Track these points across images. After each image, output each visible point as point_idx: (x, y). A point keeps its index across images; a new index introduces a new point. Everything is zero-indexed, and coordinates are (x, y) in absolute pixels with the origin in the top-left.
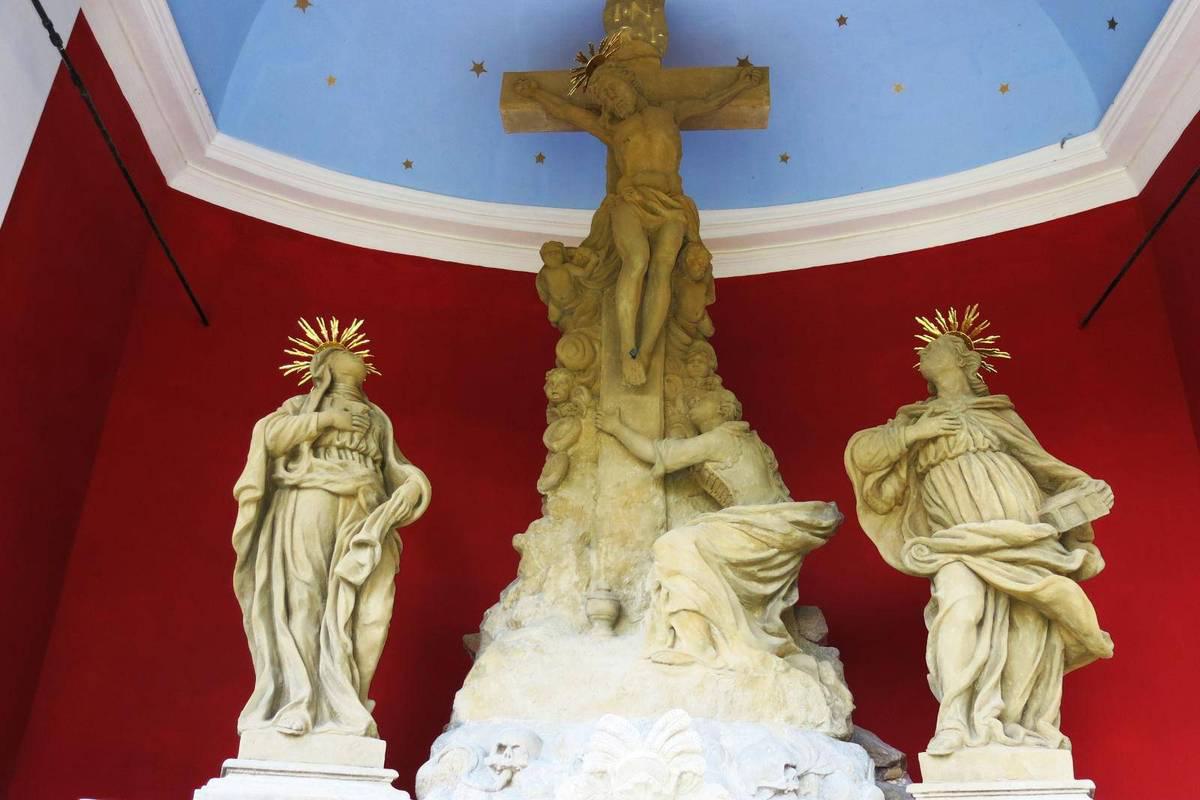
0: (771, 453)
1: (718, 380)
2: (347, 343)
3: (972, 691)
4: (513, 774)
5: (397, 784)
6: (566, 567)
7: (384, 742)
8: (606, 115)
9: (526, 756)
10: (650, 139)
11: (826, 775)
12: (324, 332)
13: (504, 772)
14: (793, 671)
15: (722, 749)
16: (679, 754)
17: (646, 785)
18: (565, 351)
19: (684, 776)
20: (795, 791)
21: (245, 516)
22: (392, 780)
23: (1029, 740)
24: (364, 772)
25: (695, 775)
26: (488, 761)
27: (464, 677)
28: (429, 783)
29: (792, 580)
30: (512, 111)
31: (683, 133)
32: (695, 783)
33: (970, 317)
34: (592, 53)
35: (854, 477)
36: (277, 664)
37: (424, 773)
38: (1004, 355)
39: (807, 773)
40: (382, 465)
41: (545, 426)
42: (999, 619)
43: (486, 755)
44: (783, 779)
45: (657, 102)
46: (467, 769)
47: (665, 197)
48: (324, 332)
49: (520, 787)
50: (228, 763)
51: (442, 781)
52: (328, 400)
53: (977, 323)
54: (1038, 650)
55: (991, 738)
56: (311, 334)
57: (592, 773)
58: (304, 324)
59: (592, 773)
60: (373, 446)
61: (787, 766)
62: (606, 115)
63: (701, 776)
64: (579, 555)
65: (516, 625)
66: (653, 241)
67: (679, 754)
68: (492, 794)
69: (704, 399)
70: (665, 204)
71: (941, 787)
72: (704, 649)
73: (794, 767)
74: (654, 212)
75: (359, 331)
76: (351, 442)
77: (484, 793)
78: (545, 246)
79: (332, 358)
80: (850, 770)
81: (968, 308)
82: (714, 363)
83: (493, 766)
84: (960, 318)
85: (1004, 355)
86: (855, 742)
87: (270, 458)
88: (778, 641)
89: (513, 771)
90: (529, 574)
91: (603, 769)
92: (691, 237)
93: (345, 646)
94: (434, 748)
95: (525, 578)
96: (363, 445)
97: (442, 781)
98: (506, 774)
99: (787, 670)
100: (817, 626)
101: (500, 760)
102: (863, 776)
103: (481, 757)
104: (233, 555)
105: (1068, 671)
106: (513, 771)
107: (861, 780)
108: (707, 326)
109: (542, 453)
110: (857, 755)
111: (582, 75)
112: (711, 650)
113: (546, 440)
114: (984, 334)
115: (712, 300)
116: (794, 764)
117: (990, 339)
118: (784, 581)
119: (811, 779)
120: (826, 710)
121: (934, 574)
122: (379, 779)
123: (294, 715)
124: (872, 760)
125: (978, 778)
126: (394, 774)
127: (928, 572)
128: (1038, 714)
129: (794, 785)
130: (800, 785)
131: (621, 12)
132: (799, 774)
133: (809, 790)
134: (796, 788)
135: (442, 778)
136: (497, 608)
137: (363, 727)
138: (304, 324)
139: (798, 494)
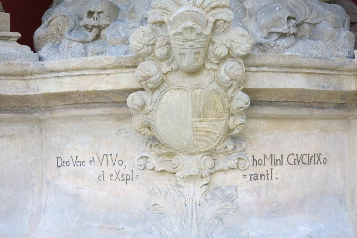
4: (100, 31)
5: (21, 41)
7: (8, 15)
9: (108, 19)
11: (316, 24)
13: (95, 30)
15: (245, 9)
16: (214, 8)
17: (192, 29)
19: (218, 23)
20: (294, 34)
22: (17, 39)
25: (225, 22)
26: (82, 23)
27: (10, 16)
28: (43, 40)
32: (225, 27)
37: (39, 33)
39: (303, 23)
43: (80, 19)
44: (286, 27)
46: (68, 29)
49: (106, 39)
51: (52, 38)
57: (154, 24)
59: (154, 24)
61: (289, 18)
63: (228, 23)
67: (214, 8)
68: (86, 44)
72: (237, 107)
73: (294, 19)
77: (81, 44)
80: (332, 21)
83: (86, 26)
86: (338, 4)
89: (100, 28)
91: (162, 20)
94: (43, 18)
97: (52, 38)
98: (95, 31)
101: (91, 22)
102: (341, 25)
103: (77, 21)
106: (100, 28)
107: (340, 27)
110: (338, 12)
116: (294, 16)
119: (306, 26)
122: (7, 39)
124: (348, 15)
126: (18, 35)
129: (293, 30)
130: (298, 31)
132: (298, 23)
133: (303, 34)
134: (295, 32)
135: (51, 36)
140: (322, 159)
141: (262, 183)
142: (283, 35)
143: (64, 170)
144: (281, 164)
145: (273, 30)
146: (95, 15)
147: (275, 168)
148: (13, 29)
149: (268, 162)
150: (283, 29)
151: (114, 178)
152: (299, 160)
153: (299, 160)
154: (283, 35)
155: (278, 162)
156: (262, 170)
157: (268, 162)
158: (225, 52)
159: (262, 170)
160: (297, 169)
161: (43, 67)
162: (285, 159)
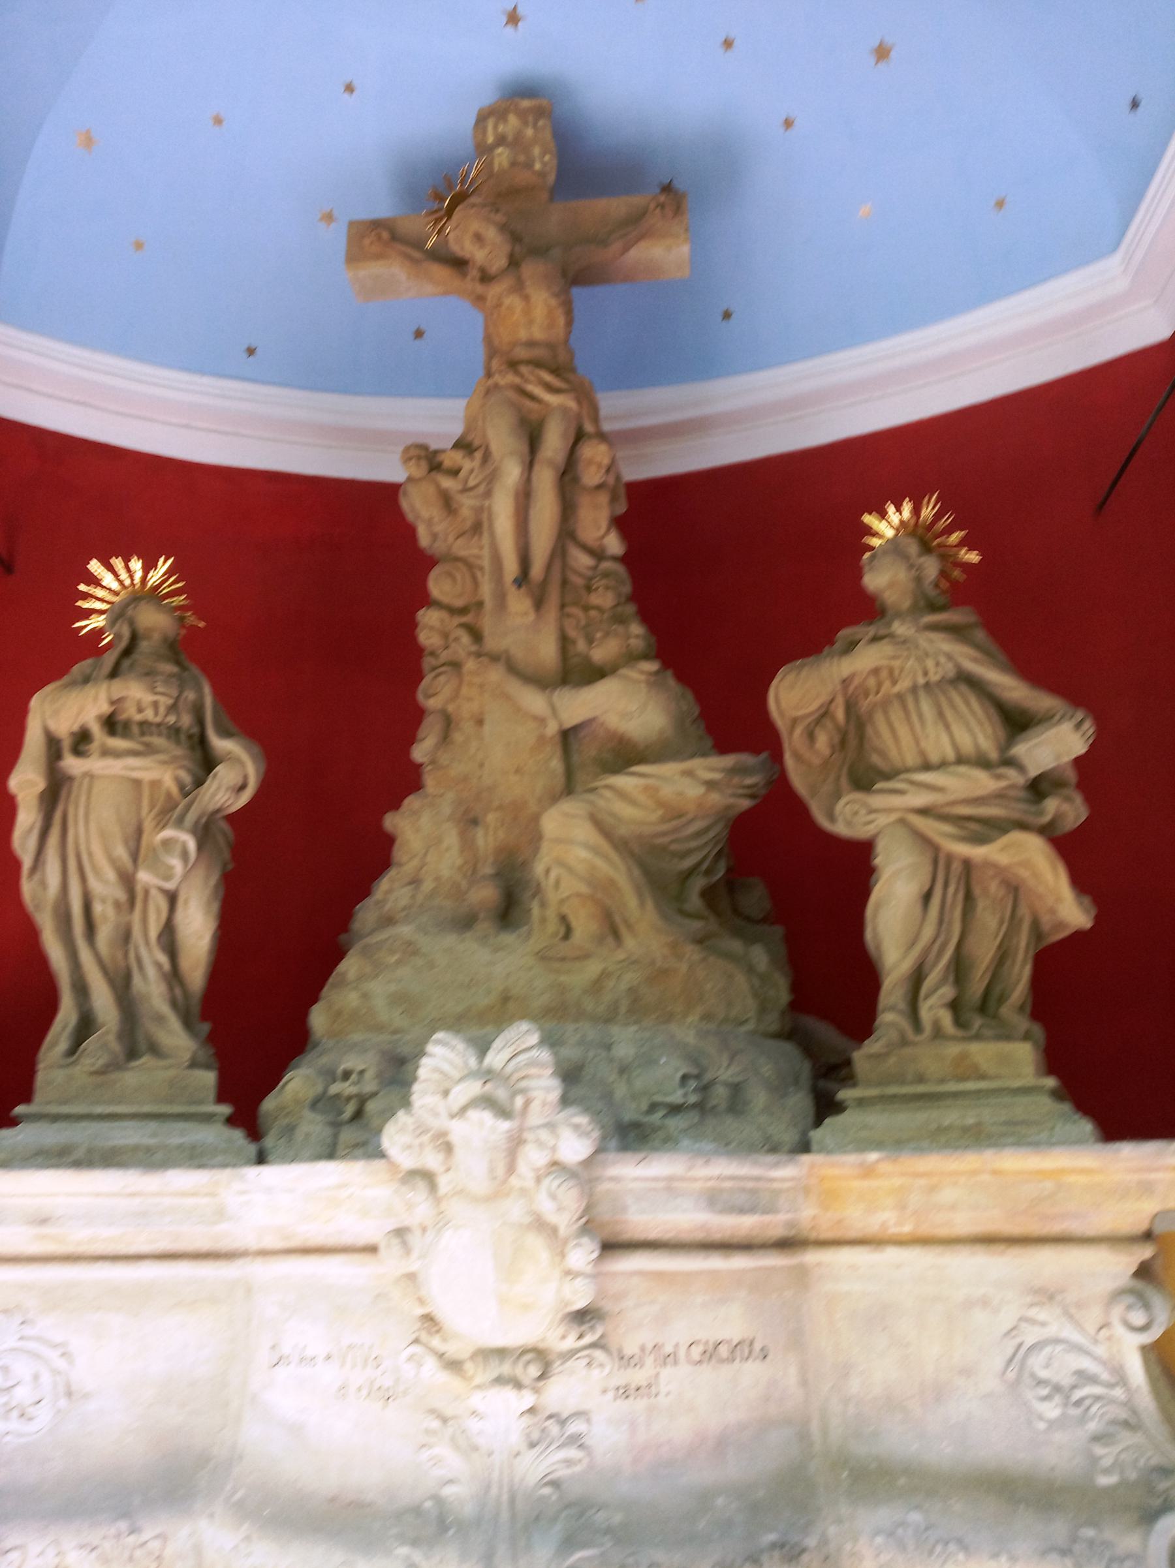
0: (690, 697)
1: (631, 609)
2: (156, 588)
3: (917, 977)
5: (231, 1121)
6: (447, 849)
8: (474, 273)
10: (526, 298)
12: (124, 575)
14: (712, 959)
18: (438, 585)
21: (27, 818)
23: (987, 1032)
24: (193, 1109)
29: (718, 848)
30: (362, 273)
31: (576, 291)
33: (927, 512)
34: (463, 182)
35: (780, 723)
36: (82, 990)
38: (973, 557)
40: (200, 743)
41: (420, 678)
42: (951, 890)
44: (680, 1092)
45: (538, 251)
47: (548, 377)
48: (124, 575)
50: (20, 1109)
52: (126, 663)
53: (938, 517)
54: (1001, 923)
55: (938, 1033)
56: (108, 579)
58: (95, 566)
60: (186, 720)
62: (474, 273)
64: (463, 834)
65: (388, 921)
66: (533, 438)
69: (607, 634)
70: (550, 389)
71: (873, 1092)
74: (532, 397)
75: (169, 573)
76: (156, 714)
78: (407, 450)
79: (135, 608)
81: (162, 560)
82: (627, 589)
84: (916, 511)
85: (973, 557)
87: (53, 747)
88: (697, 925)
90: (404, 859)
92: (589, 427)
93: (159, 966)
95: (400, 865)
96: (172, 719)
99: (704, 959)
100: (756, 897)
104: (16, 864)
105: (1040, 947)
108: (614, 544)
109: (418, 715)
111: (441, 219)
112: (610, 940)
113: (420, 696)
114: (948, 531)
115: (622, 508)
117: (955, 537)
118: (704, 852)
120: (751, 1004)
121: (876, 836)
122: (208, 1118)
123: (96, 1049)
125: (921, 1079)
126: (225, 1110)
127: (872, 833)
128: (1002, 999)
129: (693, 1099)
131: (495, 127)
136: (369, 902)
137: (187, 1056)
138: (95, 566)
139: (723, 747)
140: (757, 1346)
141: (639, 1405)
142: (675, 1109)
143: (282, 1372)
144: (676, 1362)
145: (658, 1098)
146: (354, 1077)
147: (667, 1372)
148: (221, 1098)
149: (649, 1361)
150: (677, 1097)
151: (364, 1392)
152: (711, 1353)
153: (711, 1353)
154: (675, 1109)
155: (670, 1359)
156: (638, 1376)
157: (649, 1361)
158: (847, 804)
159: (638, 1376)
160: (707, 1373)
161: (428, 886)
162: (682, 1353)
